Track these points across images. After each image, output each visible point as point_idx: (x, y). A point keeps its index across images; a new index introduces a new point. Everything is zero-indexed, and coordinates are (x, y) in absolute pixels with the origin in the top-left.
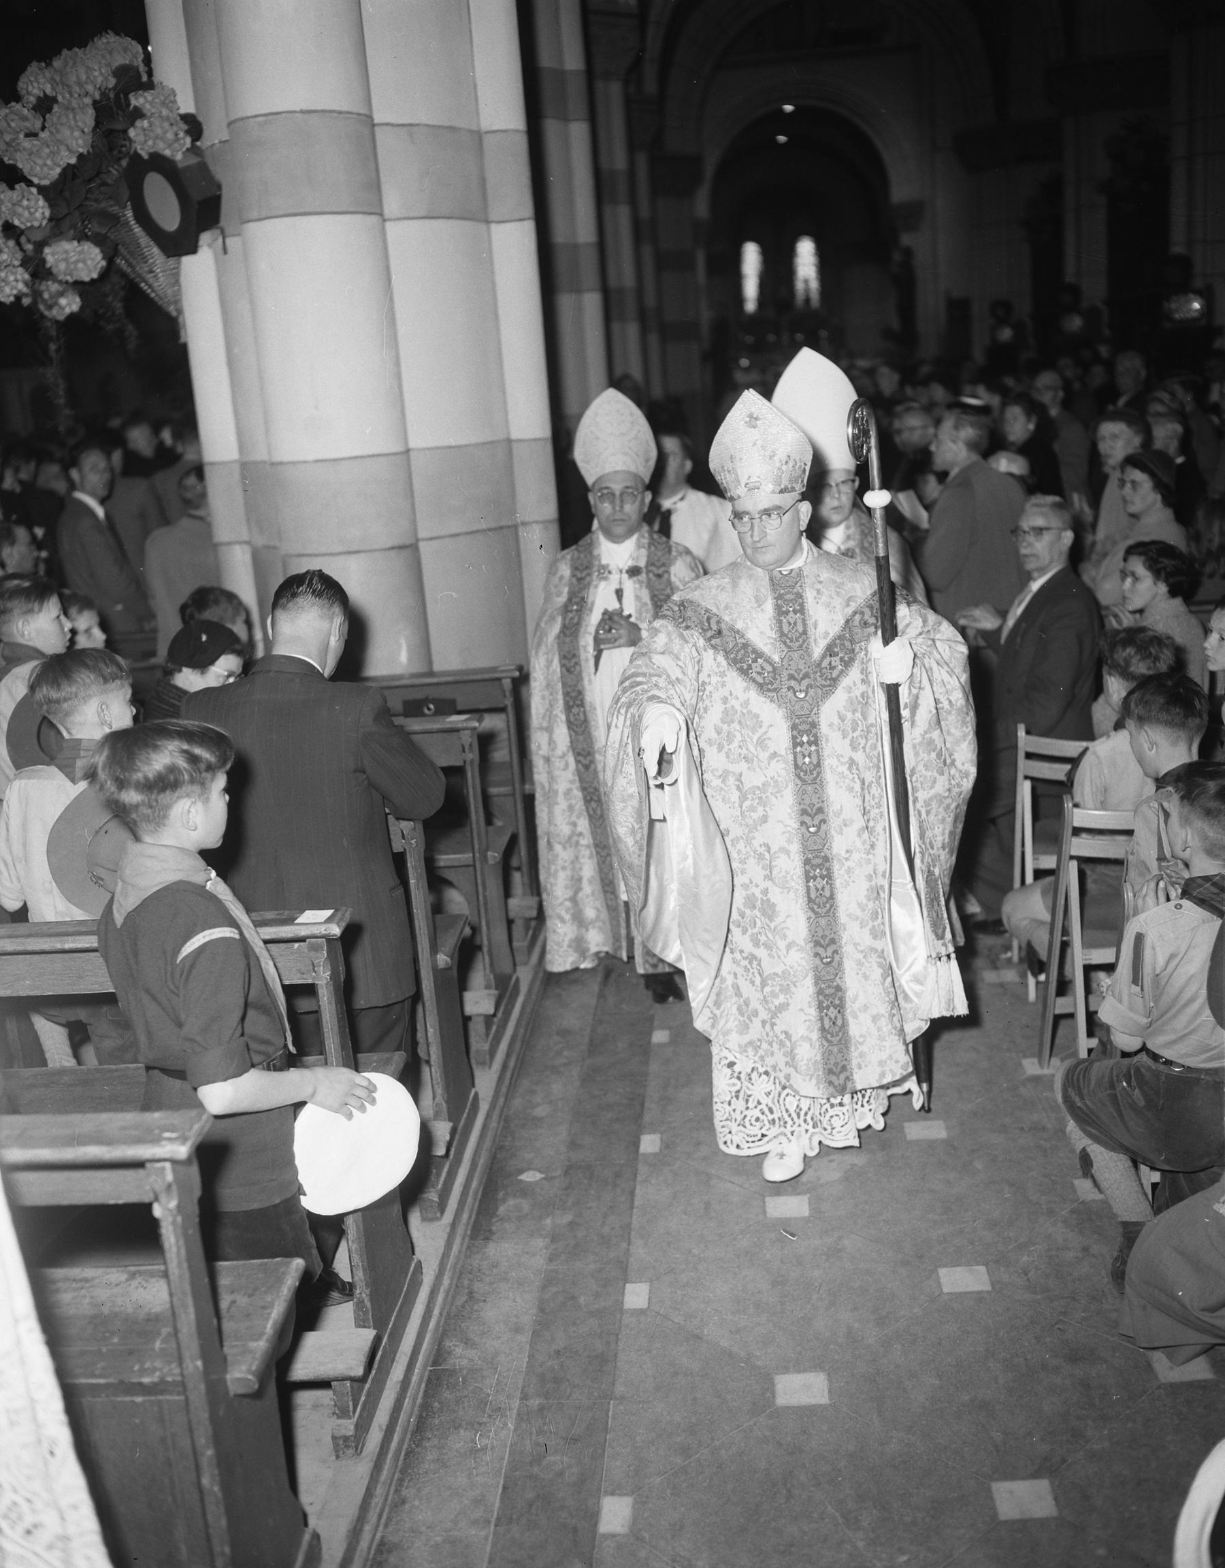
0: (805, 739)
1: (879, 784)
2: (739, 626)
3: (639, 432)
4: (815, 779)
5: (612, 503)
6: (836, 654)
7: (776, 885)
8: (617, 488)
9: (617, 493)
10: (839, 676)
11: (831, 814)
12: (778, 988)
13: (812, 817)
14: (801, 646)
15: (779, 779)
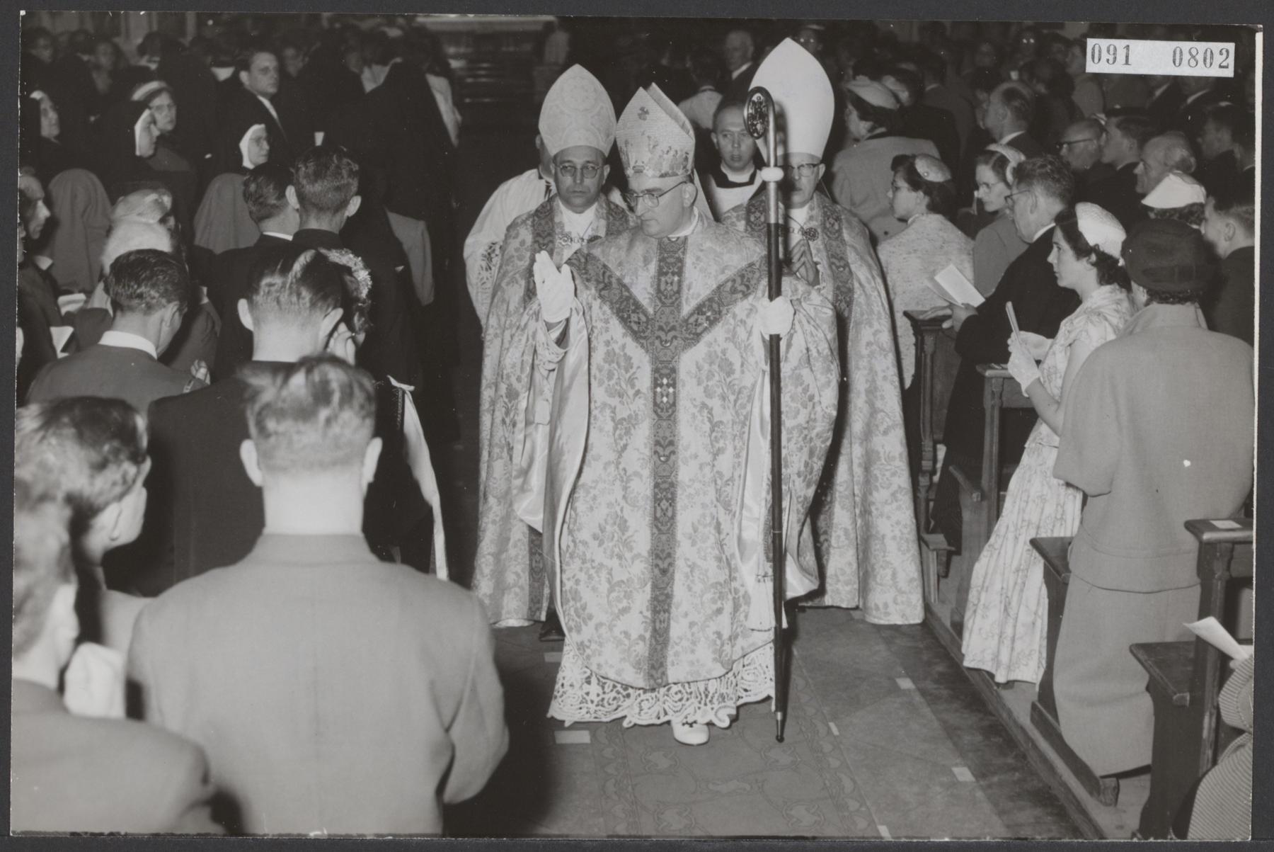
0: (665, 381)
1: (741, 438)
2: (627, 281)
3: (602, 108)
4: (670, 416)
5: (574, 175)
6: (703, 313)
7: (629, 505)
8: (579, 161)
9: (579, 167)
10: (702, 332)
11: (680, 447)
12: (623, 594)
13: (664, 448)
14: (673, 303)
15: (639, 413)
